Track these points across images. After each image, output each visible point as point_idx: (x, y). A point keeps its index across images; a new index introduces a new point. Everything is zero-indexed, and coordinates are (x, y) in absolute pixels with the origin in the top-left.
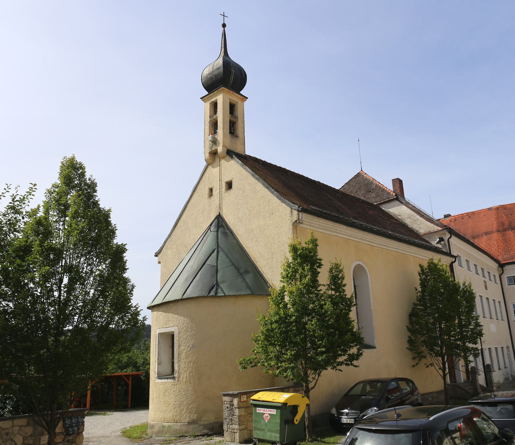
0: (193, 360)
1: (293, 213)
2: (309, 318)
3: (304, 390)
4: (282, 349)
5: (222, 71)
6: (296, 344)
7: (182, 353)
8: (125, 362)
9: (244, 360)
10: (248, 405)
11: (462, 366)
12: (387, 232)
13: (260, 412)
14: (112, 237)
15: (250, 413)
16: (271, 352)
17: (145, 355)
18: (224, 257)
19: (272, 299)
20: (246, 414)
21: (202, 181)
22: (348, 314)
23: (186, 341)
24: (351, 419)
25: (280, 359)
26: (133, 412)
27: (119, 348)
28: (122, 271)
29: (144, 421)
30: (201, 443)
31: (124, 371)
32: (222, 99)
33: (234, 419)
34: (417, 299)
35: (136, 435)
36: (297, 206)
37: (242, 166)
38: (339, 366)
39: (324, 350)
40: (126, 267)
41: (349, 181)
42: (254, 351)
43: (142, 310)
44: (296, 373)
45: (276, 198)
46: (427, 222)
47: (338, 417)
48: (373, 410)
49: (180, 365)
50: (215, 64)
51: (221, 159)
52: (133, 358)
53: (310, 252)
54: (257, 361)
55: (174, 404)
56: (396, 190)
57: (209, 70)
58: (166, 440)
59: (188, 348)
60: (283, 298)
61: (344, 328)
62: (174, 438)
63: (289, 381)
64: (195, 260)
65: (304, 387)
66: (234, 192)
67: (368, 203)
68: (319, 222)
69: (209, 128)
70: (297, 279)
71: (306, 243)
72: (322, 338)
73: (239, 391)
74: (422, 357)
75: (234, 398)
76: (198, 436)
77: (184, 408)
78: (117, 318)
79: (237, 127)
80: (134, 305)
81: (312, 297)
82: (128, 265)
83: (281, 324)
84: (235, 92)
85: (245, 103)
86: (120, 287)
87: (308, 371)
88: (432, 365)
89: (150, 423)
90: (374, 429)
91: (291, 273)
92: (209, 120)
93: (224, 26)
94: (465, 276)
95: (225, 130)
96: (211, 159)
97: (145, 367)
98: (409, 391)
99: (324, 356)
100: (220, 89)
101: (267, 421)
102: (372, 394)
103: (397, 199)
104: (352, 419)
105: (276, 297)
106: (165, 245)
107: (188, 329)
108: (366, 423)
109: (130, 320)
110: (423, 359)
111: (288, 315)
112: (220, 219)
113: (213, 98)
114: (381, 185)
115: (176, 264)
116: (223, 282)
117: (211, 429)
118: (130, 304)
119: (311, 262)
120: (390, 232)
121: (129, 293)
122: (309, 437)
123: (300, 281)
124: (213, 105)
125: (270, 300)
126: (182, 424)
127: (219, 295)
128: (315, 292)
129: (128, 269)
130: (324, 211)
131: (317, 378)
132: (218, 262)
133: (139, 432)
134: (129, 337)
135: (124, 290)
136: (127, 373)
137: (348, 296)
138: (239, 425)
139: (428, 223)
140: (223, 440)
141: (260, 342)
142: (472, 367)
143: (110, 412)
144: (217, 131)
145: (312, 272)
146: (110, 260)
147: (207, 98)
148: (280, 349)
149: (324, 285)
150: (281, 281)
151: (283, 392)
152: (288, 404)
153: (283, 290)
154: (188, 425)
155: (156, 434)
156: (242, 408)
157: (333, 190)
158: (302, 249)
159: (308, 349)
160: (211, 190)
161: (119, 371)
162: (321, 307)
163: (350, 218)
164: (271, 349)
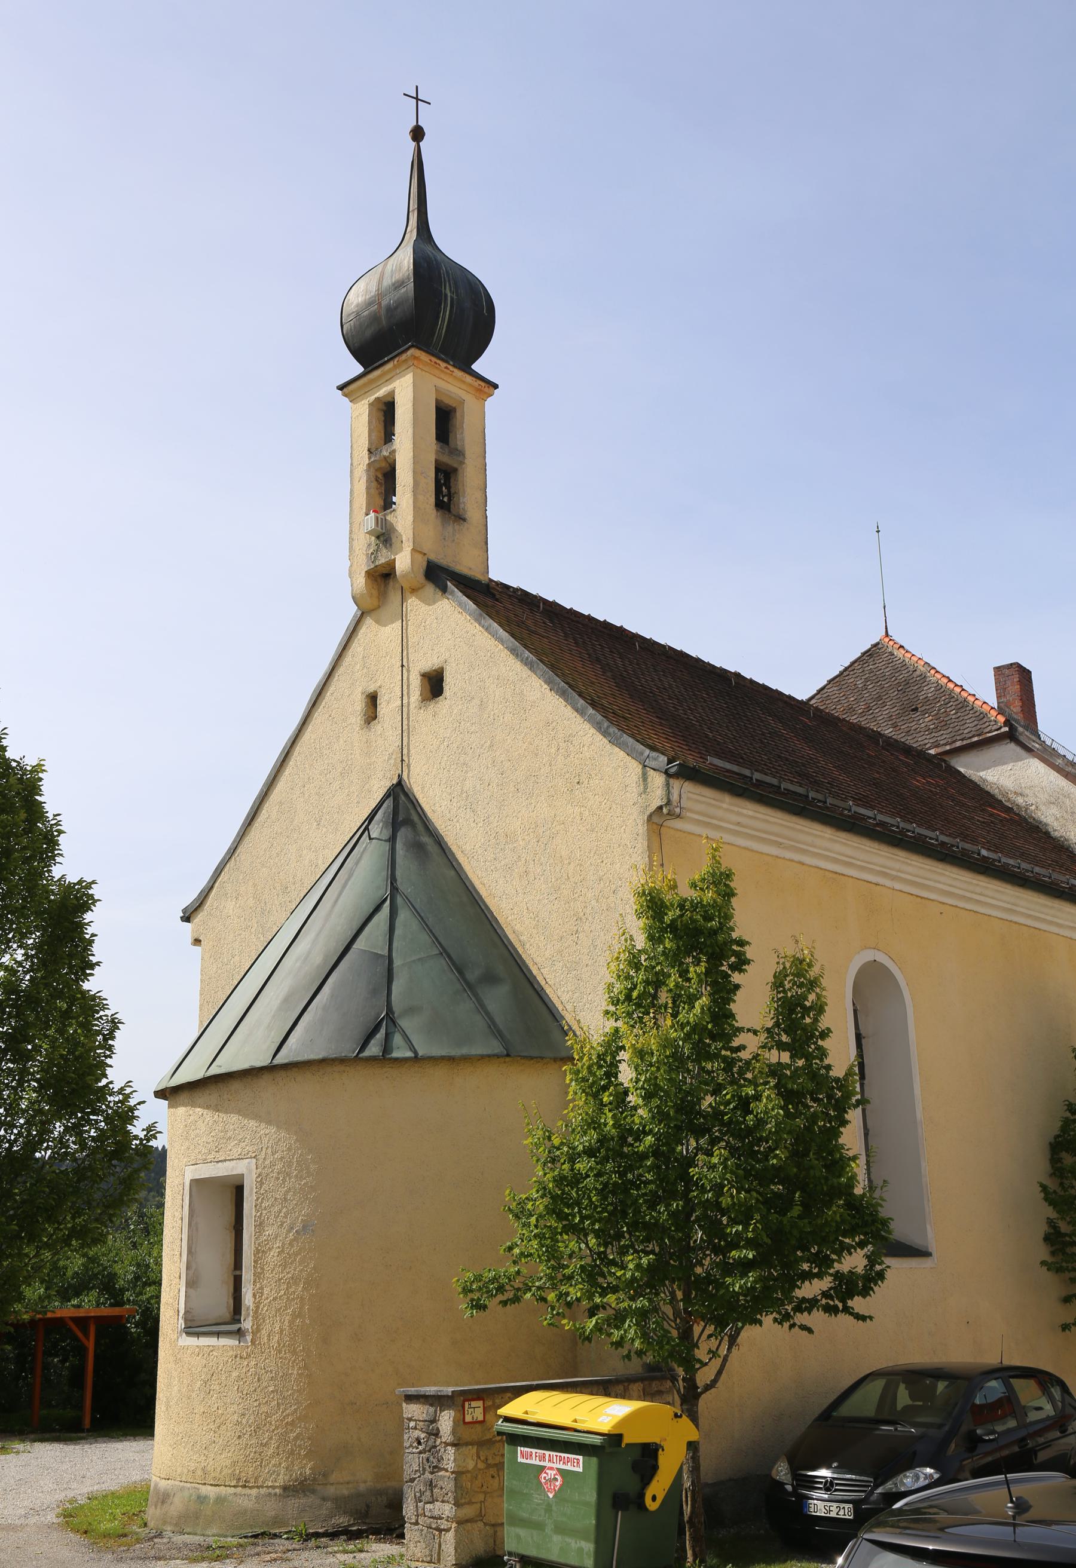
0: (304, 1274)
1: (649, 779)
2: (702, 1141)
3: (678, 1391)
4: (606, 1245)
5: (411, 294)
6: (653, 1230)
7: (270, 1249)
8: (76, 1273)
9: (478, 1278)
10: (488, 1437)
12: (973, 852)
13: (528, 1461)
14: (47, 856)
15: (496, 1465)
16: (570, 1256)
17: (142, 1251)
18: (415, 924)
19: (578, 1072)
20: (481, 1465)
21: (340, 670)
22: (837, 1134)
23: (284, 1210)
24: (842, 1505)
25: (600, 1280)
26: (98, 1445)
27: (66, 1228)
28: (77, 972)
29: (136, 1476)
30: (328, 1561)
31: (73, 1306)
32: (410, 389)
33: (440, 1483)
35: (109, 1526)
36: (663, 759)
37: (476, 620)
38: (801, 1311)
39: (751, 1256)
40: (91, 958)
41: (841, 673)
42: (510, 1249)
43: (144, 1102)
44: (654, 1330)
45: (593, 731)
47: (794, 1491)
48: (922, 1476)
49: (262, 1288)
50: (389, 267)
51: (407, 594)
52: (104, 1260)
53: (708, 918)
54: (521, 1286)
55: (238, 1423)
56: (1008, 704)
57: (367, 291)
58: (209, 1547)
59: (289, 1231)
60: (612, 1072)
61: (823, 1181)
62: (235, 1541)
63: (628, 1357)
64: (318, 935)
65: (681, 1382)
66: (450, 707)
67: (907, 750)
68: (739, 814)
69: (368, 488)
70: (660, 1007)
71: (694, 885)
72: (744, 1216)
73: (457, 1385)
75: (441, 1411)
76: (317, 1535)
77: (271, 1438)
78: (59, 1127)
79: (460, 487)
80: (116, 1087)
81: (713, 1072)
82: (98, 952)
83: (606, 1159)
84: (454, 366)
86: (71, 1025)
87: (695, 1325)
89: (156, 1485)
90: (931, 1548)
91: (640, 988)
92: (367, 461)
93: (418, 134)
95: (421, 497)
96: (371, 595)
97: (141, 1293)
98: (1048, 1418)
99: (752, 1276)
100: (404, 357)
101: (551, 1496)
102: (920, 1420)
103: (1011, 736)
104: (847, 1506)
105: (589, 1068)
106: (217, 885)
107: (290, 1166)
108: (901, 1525)
109: (102, 1136)
111: (630, 1131)
112: (402, 797)
113: (379, 387)
114: (956, 685)
115: (253, 947)
116: (411, 1011)
117: (362, 1515)
118: (104, 1082)
119: (710, 951)
120: (984, 852)
121: (100, 1047)
122: (694, 1561)
123: (675, 1015)
124: (379, 409)
125: (568, 1078)
126: (263, 1491)
128: (723, 1052)
129: (98, 964)
130: (757, 776)
131: (723, 1351)
132: (395, 944)
133: (119, 1516)
134: (97, 1196)
135: (86, 1036)
136: (81, 1310)
137: (838, 1072)
138: (457, 1504)
140: (402, 1556)
141: (533, 1220)
143: (23, 1441)
144: (394, 499)
145: (714, 984)
146: (38, 934)
147: (360, 388)
148: (599, 1245)
149: (755, 1032)
150: (607, 1012)
151: (607, 1394)
152: (626, 1440)
153: (613, 1045)
154: (284, 1497)
155: (176, 1525)
156: (467, 1444)
157: (785, 702)
158: (681, 906)
159: (693, 1249)
160: (373, 699)
161: (56, 1304)
162: (744, 1105)
163: (844, 800)
164: (570, 1244)
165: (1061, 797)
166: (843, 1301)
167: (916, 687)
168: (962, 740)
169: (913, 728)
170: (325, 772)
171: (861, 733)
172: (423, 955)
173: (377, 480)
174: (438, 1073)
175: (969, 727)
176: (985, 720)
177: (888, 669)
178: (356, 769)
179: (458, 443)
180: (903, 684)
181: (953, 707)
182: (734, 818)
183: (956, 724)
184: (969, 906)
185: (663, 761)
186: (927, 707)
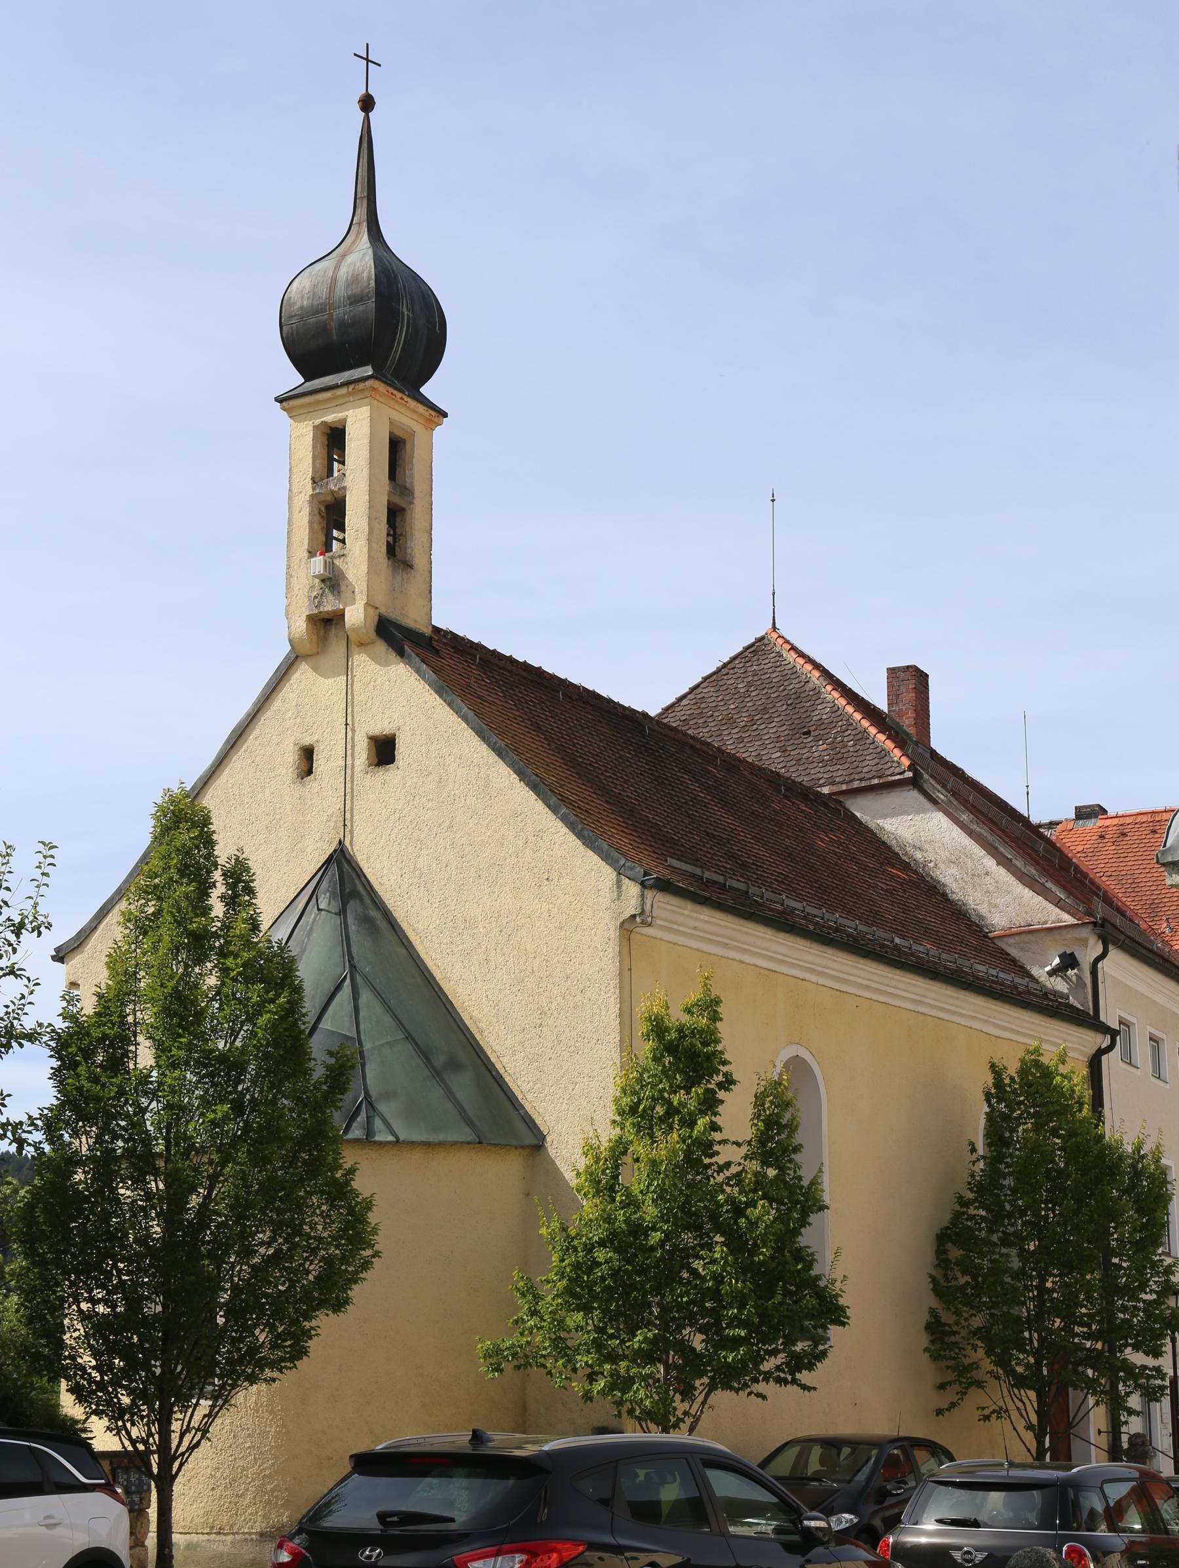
1: (624, 888)
11: (1100, 1432)
18: (377, 1007)
21: (268, 715)
32: (367, 423)
34: (969, 1183)
41: (719, 670)
45: (565, 830)
46: (1021, 886)
51: (354, 648)
66: (403, 778)
68: (697, 919)
71: (688, 1011)
74: (970, 1384)
79: (408, 529)
84: (409, 396)
85: (438, 432)
88: (1000, 1412)
92: (310, 492)
93: (367, 103)
94: (1145, 1121)
95: (374, 546)
96: (311, 643)
110: (973, 1390)
116: (387, 1095)
120: (897, 940)
124: (324, 433)
126: (238, 1537)
127: (377, 1138)
132: (362, 1027)
139: (1027, 890)
142: (1133, 1438)
147: (303, 406)
149: (738, 1144)
150: (614, 1122)
154: (261, 1542)
160: (308, 754)
165: (962, 856)
166: (792, 1374)
167: (808, 704)
168: (861, 780)
169: (804, 756)
170: (247, 822)
171: (762, 778)
172: (390, 1039)
173: (320, 514)
174: (416, 1156)
175: (869, 765)
176: (887, 759)
177: (775, 675)
178: (286, 825)
179: (407, 480)
180: (793, 697)
181: (851, 737)
182: (692, 923)
183: (854, 759)
184: (882, 999)
185: (639, 872)
186: (821, 732)
